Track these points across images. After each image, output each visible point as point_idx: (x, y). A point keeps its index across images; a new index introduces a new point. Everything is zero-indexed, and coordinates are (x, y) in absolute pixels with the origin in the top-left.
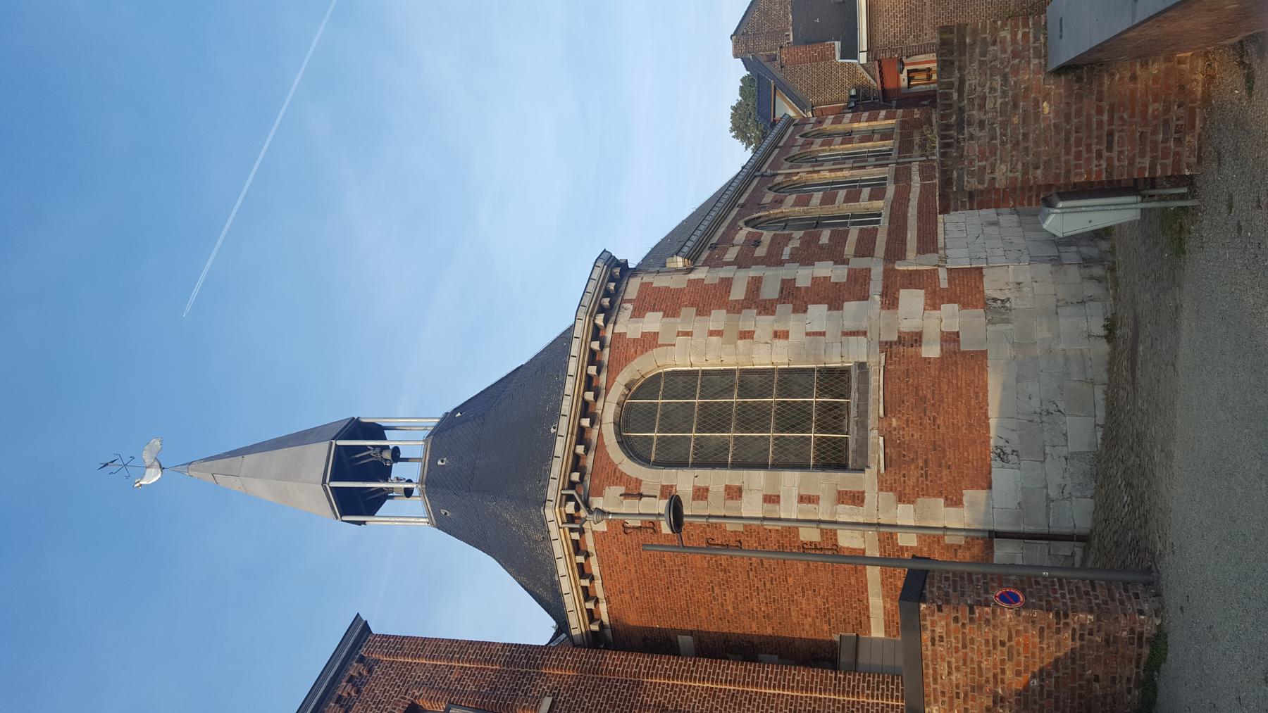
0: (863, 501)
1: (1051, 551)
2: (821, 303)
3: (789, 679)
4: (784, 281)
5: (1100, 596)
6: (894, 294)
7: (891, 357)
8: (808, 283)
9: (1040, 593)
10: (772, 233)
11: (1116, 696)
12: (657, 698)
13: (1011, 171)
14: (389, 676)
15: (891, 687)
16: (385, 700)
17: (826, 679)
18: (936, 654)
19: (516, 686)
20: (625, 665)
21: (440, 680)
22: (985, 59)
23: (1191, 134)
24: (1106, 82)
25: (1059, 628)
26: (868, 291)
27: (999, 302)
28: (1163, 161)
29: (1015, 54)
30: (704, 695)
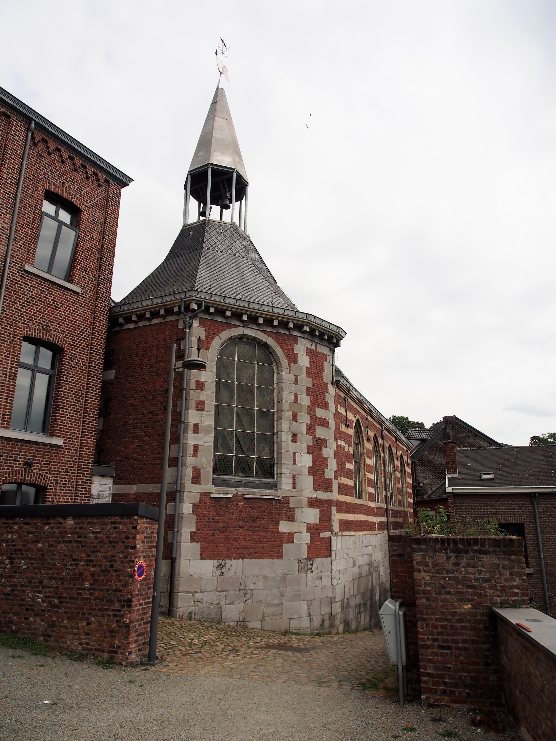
0: (194, 483)
1: (163, 594)
2: (313, 462)
3: (88, 435)
4: (325, 441)
5: (140, 627)
6: (317, 506)
7: (280, 503)
8: (324, 455)
9: (143, 590)
10: (352, 434)
11: (78, 635)
12: (79, 355)
13: (425, 583)
14: (97, 197)
15: (83, 495)
16: (82, 194)
17: (88, 457)
18: (105, 525)
19: (88, 272)
20: (98, 337)
21: (93, 227)
22: (501, 568)
23: (449, 701)
24: (485, 646)
25: (121, 602)
26: (319, 490)
27: (311, 567)
28: (431, 682)
29: (503, 588)
30: (80, 384)
